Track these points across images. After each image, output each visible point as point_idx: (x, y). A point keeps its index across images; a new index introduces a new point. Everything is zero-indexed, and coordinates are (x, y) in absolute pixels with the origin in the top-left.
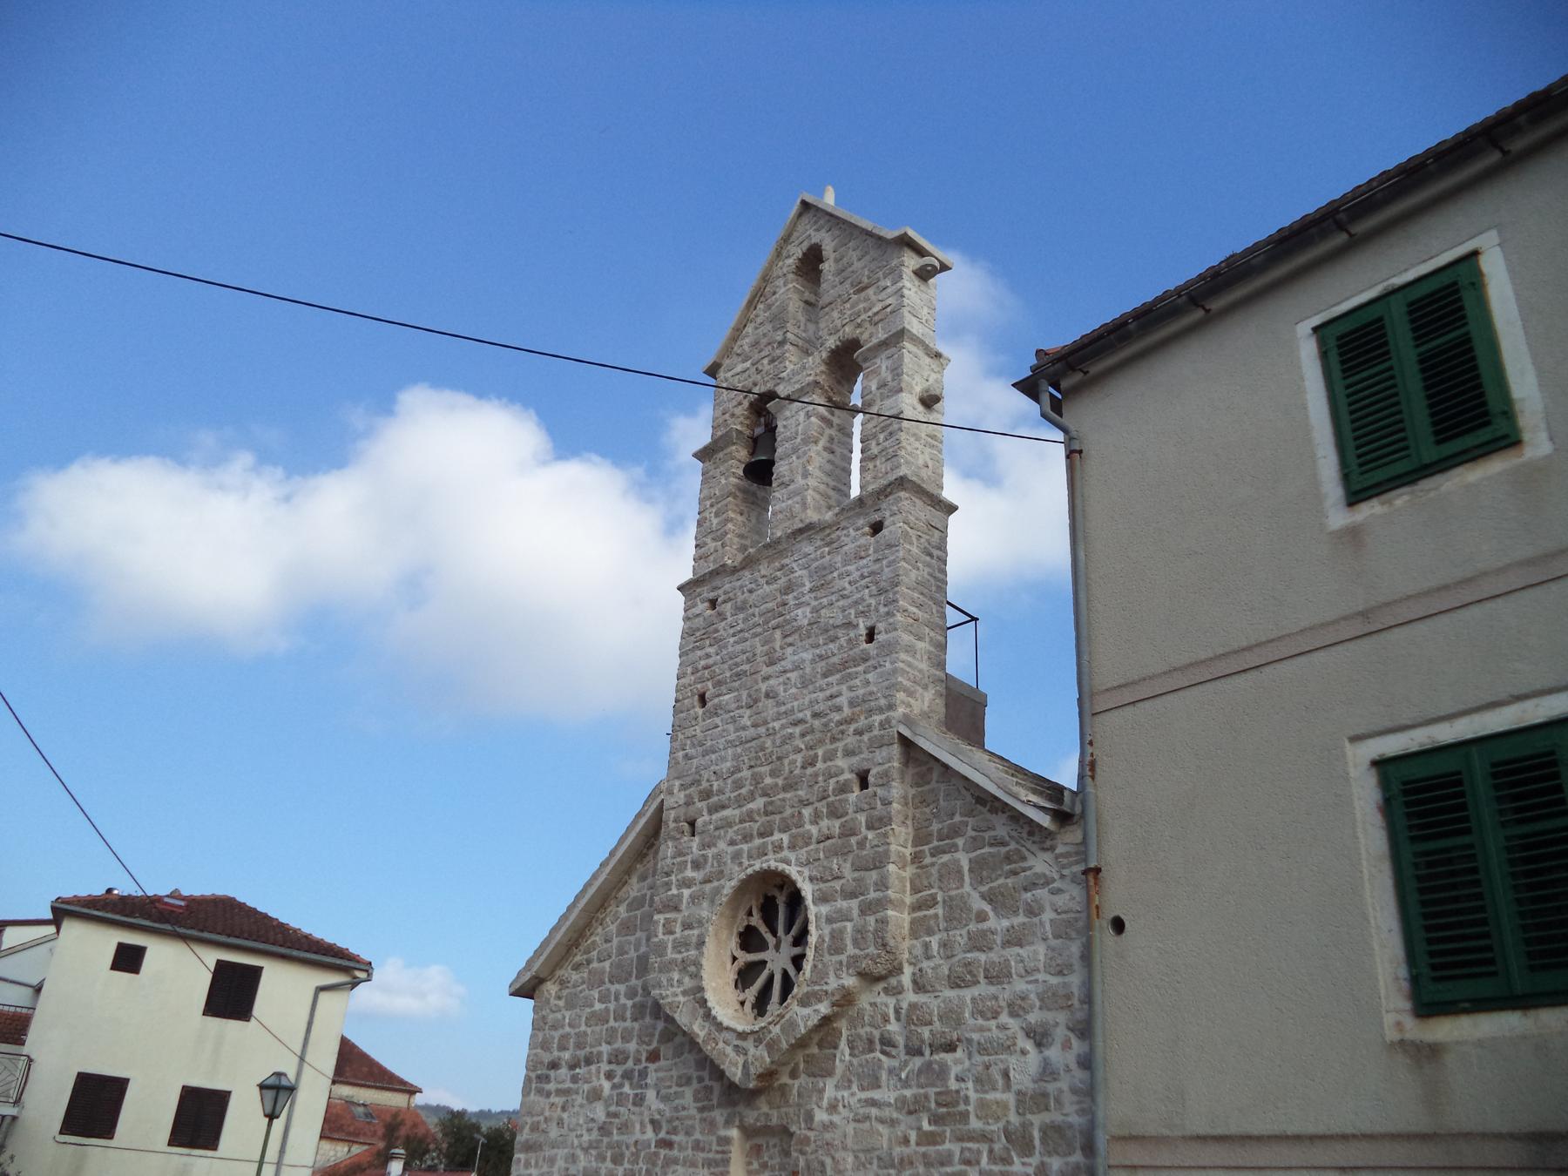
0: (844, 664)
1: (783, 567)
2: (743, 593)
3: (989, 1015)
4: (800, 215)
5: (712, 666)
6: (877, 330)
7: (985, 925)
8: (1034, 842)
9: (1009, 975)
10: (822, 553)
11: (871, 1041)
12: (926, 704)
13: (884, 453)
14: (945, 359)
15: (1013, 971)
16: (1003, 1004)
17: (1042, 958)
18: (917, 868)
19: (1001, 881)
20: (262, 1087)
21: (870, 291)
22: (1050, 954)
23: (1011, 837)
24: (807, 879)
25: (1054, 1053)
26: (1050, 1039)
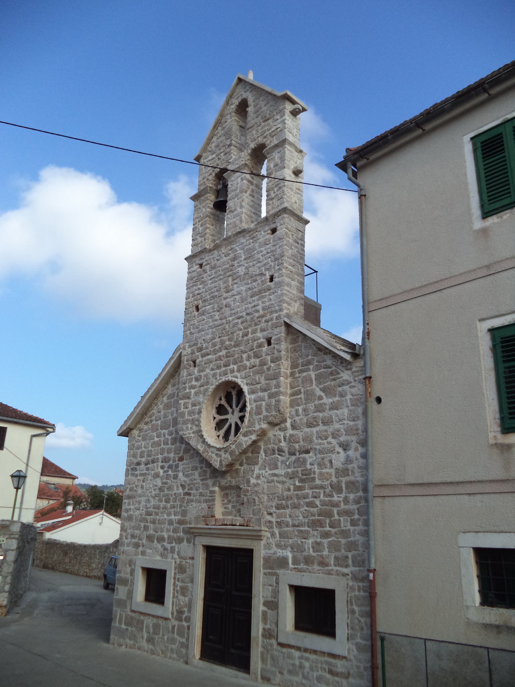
0: (260, 292)
2: (214, 261)
7: (322, 402)
9: (332, 422)
11: (274, 450)
12: (296, 309)
13: (277, 197)
14: (304, 153)
19: (328, 383)
20: (12, 476)
24: (245, 384)
26: (349, 447)
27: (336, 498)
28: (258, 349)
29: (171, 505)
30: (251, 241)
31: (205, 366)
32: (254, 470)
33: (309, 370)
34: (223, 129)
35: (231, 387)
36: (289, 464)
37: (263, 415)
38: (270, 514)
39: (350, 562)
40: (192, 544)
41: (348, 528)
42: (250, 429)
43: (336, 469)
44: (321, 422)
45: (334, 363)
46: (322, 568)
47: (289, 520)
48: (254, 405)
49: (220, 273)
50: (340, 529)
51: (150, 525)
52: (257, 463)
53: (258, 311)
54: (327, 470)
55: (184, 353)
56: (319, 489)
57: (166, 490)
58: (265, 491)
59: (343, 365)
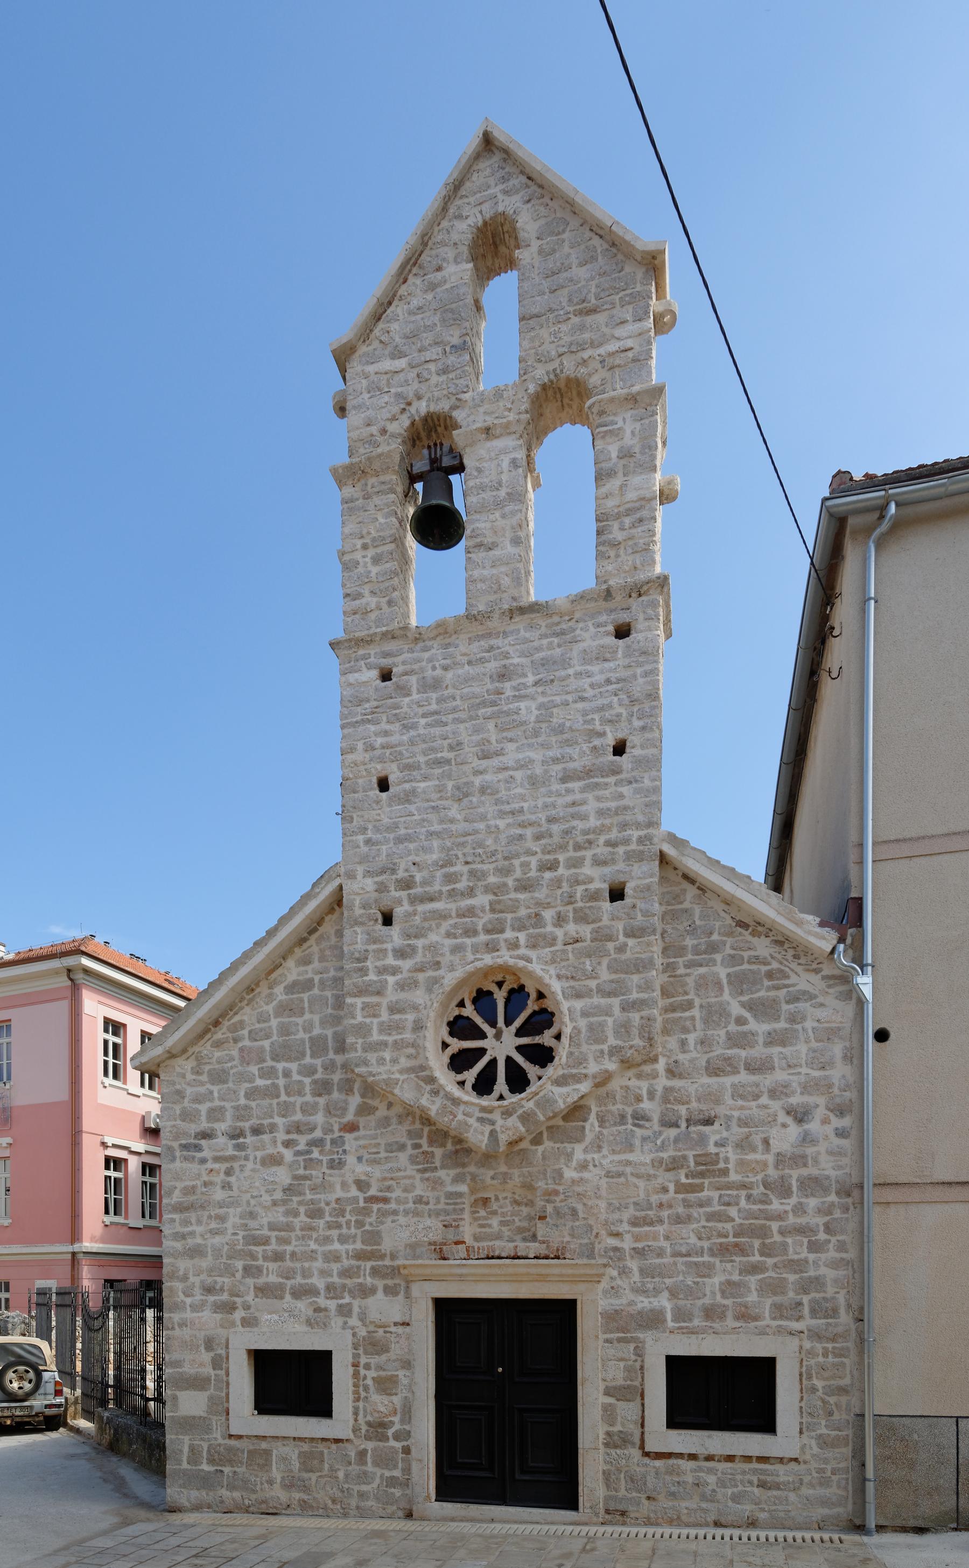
0: (588, 773)
1: (491, 649)
2: (434, 668)
3: (750, 1098)
4: (477, 157)
5: (396, 746)
6: (613, 377)
7: (745, 1028)
8: (799, 964)
9: (773, 1068)
10: (551, 643)
11: (623, 1117)
13: (630, 543)
15: (776, 1065)
16: (765, 1090)
17: (804, 1056)
18: (669, 977)
21: (601, 318)
22: (811, 1055)
23: (772, 957)
24: (554, 977)
26: (810, 1117)
27: (776, 1205)
28: (588, 905)
29: (328, 1222)
30: (556, 640)
31: (426, 925)
32: (572, 1153)
33: (714, 962)
34: (432, 287)
36: (663, 1142)
37: (609, 1044)
38: (617, 1235)
39: (806, 1311)
40: (401, 1297)
41: (803, 1256)
42: (574, 1071)
44: (742, 1067)
45: (776, 955)
46: (744, 1325)
47: (665, 1244)
48: (582, 1023)
49: (454, 704)
50: (785, 1258)
51: (266, 1264)
52: (579, 1140)
53: (584, 817)
54: (758, 1156)
55: (350, 888)
56: (737, 1189)
57: (308, 1192)
58: (604, 1193)
59: (800, 961)
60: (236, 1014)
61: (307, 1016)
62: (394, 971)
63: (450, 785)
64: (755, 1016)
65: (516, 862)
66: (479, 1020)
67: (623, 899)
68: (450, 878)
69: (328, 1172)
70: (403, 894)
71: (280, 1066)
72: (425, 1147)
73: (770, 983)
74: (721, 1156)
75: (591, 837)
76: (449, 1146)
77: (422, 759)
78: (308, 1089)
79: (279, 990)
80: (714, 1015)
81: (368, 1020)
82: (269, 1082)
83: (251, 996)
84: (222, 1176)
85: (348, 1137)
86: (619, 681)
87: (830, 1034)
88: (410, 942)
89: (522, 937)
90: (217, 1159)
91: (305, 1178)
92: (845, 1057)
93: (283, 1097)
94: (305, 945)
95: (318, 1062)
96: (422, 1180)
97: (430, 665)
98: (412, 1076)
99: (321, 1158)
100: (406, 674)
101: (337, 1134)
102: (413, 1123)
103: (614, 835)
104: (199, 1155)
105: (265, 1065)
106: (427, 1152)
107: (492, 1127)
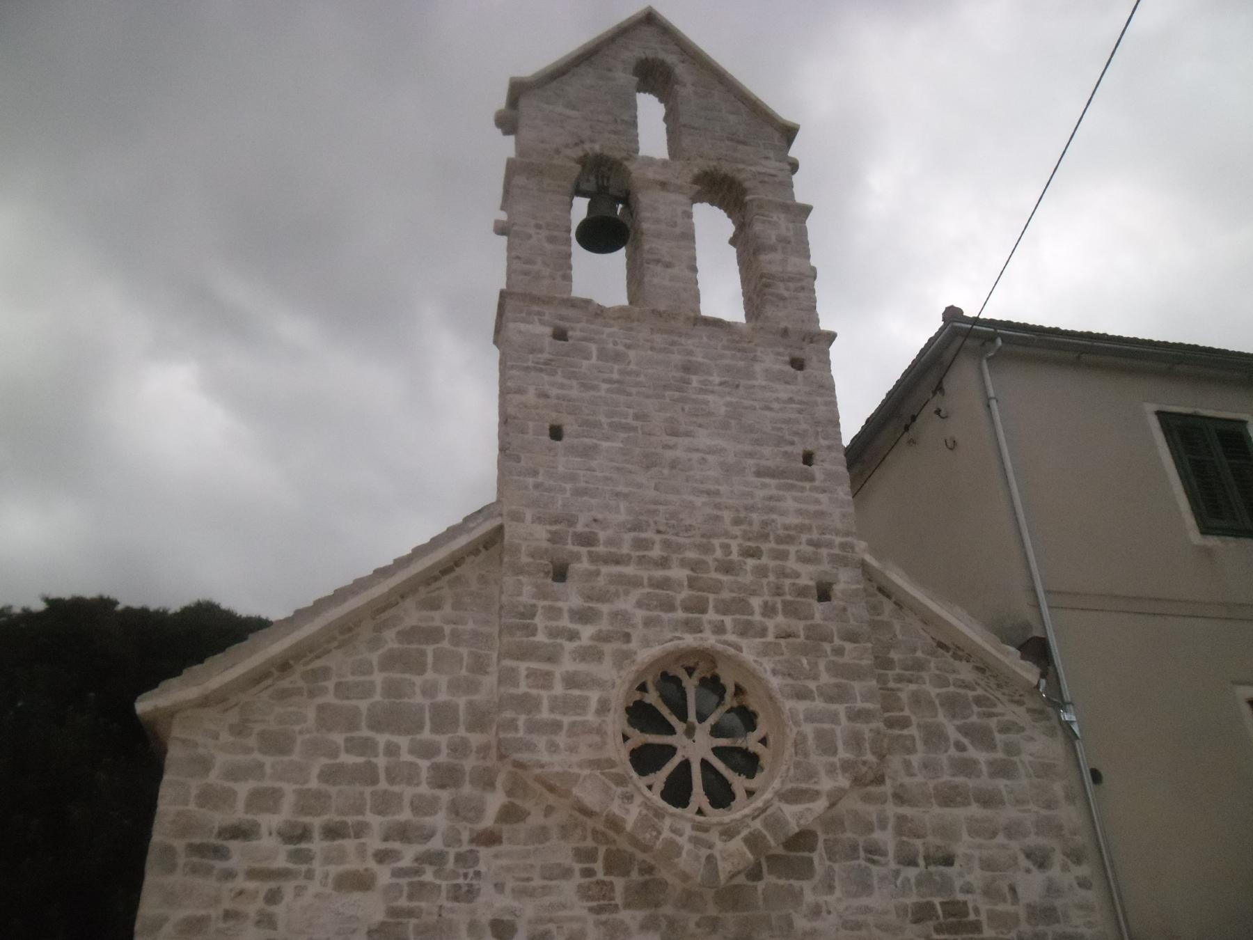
7: (965, 755)
25: (1055, 872)
35: (682, 666)
42: (804, 786)
43: (1029, 906)
45: (981, 682)
48: (808, 729)
60: (318, 657)
61: (430, 675)
62: (573, 636)
63: (637, 450)
64: (972, 743)
65: (716, 542)
66: (665, 711)
67: (829, 600)
68: (640, 544)
69: (448, 904)
70: (583, 550)
71: (382, 739)
72: (601, 876)
73: (980, 709)
74: (970, 905)
75: (792, 533)
76: (635, 876)
77: (604, 420)
78: (424, 774)
79: (390, 635)
80: (934, 737)
81: (534, 692)
82: (361, 760)
83: (347, 636)
84: (260, 903)
85: (484, 852)
86: (801, 403)
87: (1045, 770)
88: (591, 605)
89: (728, 620)
90: (252, 874)
91: (410, 913)
92: (1067, 797)
93: (383, 785)
94: (435, 585)
95: (443, 740)
96: (598, 924)
97: (611, 339)
98: (598, 772)
99: (438, 882)
100: (584, 339)
101: (465, 847)
102: (584, 838)
103: (815, 536)
104: (219, 865)
105: (356, 734)
106: (603, 883)
107: (708, 852)
